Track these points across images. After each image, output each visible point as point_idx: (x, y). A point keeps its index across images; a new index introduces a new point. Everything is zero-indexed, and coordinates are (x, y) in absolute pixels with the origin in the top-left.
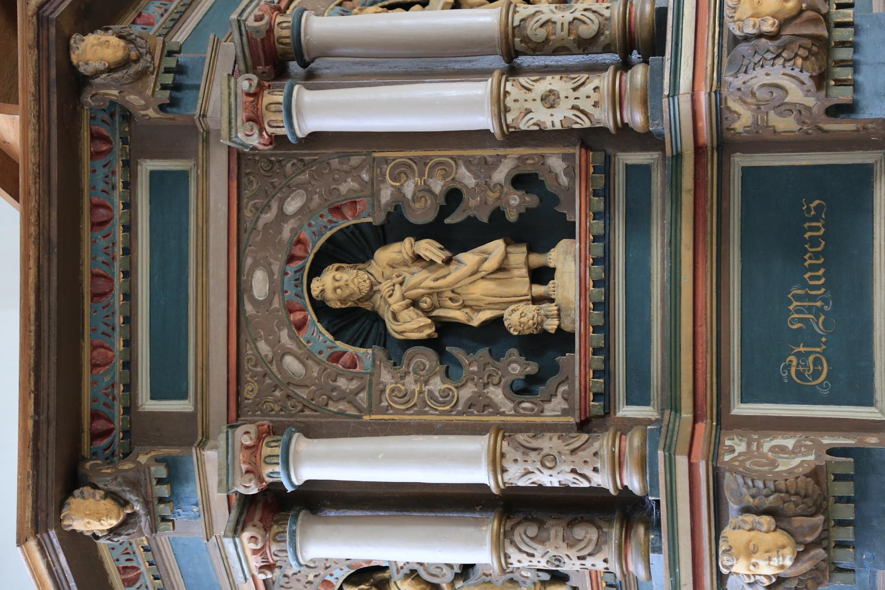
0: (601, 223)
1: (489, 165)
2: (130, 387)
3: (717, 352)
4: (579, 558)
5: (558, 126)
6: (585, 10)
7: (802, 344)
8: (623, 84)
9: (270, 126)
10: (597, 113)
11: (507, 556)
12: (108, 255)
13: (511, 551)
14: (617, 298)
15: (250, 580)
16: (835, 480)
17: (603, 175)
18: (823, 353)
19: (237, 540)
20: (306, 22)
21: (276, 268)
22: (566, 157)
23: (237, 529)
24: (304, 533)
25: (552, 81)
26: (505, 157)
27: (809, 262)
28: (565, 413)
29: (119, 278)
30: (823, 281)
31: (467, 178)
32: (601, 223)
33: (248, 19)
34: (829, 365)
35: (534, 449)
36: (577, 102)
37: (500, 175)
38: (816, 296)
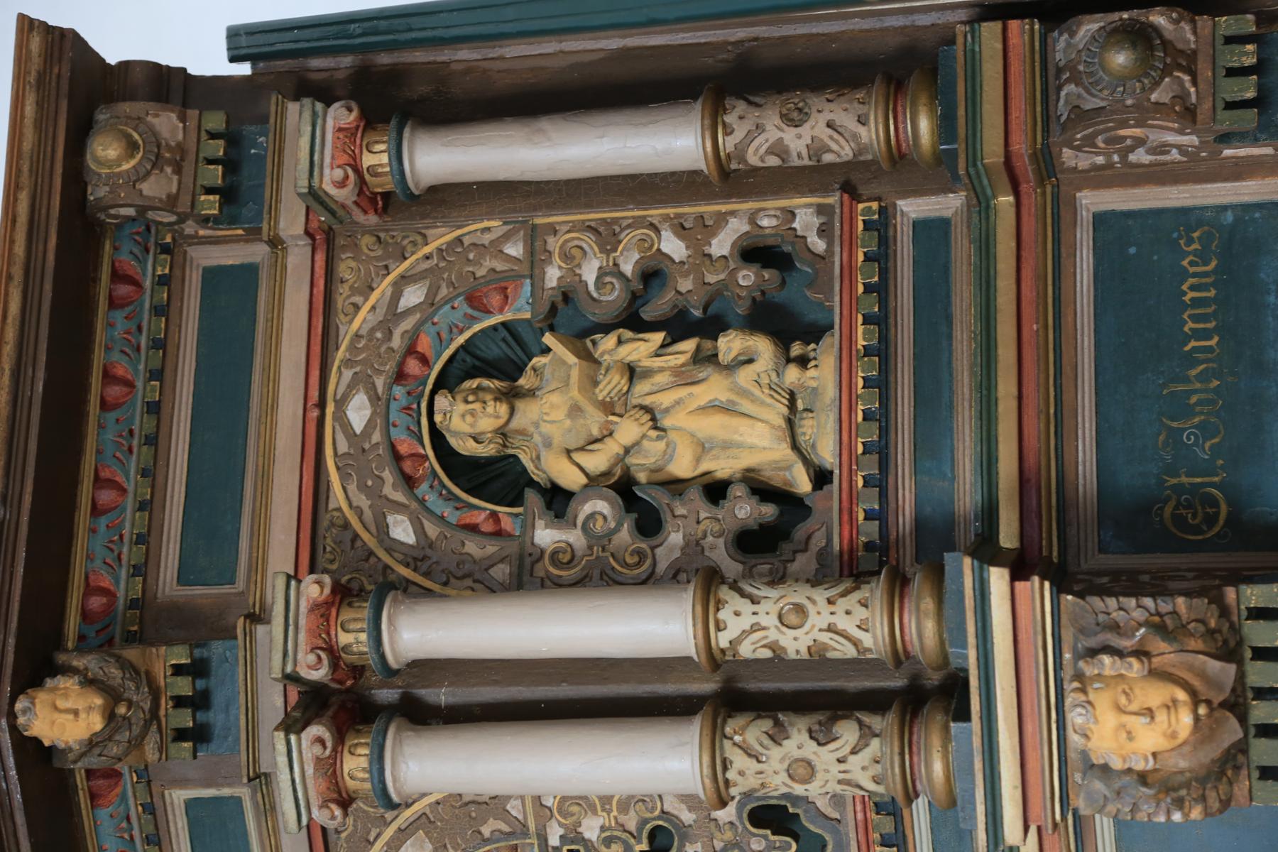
0: (875, 426)
1: (708, 228)
5: (805, 656)
8: (907, 638)
10: (867, 640)
12: (112, 550)
14: (899, 416)
15: (304, 831)
17: (876, 359)
19: (293, 738)
20: (395, 781)
21: (380, 383)
22: (821, 210)
23: (292, 725)
24: (398, 742)
26: (733, 213)
27: (1191, 295)
29: (131, 480)
30: (1212, 293)
31: (673, 246)
33: (313, 816)
35: (778, 600)
36: (832, 619)
37: (721, 245)
38: (1206, 284)
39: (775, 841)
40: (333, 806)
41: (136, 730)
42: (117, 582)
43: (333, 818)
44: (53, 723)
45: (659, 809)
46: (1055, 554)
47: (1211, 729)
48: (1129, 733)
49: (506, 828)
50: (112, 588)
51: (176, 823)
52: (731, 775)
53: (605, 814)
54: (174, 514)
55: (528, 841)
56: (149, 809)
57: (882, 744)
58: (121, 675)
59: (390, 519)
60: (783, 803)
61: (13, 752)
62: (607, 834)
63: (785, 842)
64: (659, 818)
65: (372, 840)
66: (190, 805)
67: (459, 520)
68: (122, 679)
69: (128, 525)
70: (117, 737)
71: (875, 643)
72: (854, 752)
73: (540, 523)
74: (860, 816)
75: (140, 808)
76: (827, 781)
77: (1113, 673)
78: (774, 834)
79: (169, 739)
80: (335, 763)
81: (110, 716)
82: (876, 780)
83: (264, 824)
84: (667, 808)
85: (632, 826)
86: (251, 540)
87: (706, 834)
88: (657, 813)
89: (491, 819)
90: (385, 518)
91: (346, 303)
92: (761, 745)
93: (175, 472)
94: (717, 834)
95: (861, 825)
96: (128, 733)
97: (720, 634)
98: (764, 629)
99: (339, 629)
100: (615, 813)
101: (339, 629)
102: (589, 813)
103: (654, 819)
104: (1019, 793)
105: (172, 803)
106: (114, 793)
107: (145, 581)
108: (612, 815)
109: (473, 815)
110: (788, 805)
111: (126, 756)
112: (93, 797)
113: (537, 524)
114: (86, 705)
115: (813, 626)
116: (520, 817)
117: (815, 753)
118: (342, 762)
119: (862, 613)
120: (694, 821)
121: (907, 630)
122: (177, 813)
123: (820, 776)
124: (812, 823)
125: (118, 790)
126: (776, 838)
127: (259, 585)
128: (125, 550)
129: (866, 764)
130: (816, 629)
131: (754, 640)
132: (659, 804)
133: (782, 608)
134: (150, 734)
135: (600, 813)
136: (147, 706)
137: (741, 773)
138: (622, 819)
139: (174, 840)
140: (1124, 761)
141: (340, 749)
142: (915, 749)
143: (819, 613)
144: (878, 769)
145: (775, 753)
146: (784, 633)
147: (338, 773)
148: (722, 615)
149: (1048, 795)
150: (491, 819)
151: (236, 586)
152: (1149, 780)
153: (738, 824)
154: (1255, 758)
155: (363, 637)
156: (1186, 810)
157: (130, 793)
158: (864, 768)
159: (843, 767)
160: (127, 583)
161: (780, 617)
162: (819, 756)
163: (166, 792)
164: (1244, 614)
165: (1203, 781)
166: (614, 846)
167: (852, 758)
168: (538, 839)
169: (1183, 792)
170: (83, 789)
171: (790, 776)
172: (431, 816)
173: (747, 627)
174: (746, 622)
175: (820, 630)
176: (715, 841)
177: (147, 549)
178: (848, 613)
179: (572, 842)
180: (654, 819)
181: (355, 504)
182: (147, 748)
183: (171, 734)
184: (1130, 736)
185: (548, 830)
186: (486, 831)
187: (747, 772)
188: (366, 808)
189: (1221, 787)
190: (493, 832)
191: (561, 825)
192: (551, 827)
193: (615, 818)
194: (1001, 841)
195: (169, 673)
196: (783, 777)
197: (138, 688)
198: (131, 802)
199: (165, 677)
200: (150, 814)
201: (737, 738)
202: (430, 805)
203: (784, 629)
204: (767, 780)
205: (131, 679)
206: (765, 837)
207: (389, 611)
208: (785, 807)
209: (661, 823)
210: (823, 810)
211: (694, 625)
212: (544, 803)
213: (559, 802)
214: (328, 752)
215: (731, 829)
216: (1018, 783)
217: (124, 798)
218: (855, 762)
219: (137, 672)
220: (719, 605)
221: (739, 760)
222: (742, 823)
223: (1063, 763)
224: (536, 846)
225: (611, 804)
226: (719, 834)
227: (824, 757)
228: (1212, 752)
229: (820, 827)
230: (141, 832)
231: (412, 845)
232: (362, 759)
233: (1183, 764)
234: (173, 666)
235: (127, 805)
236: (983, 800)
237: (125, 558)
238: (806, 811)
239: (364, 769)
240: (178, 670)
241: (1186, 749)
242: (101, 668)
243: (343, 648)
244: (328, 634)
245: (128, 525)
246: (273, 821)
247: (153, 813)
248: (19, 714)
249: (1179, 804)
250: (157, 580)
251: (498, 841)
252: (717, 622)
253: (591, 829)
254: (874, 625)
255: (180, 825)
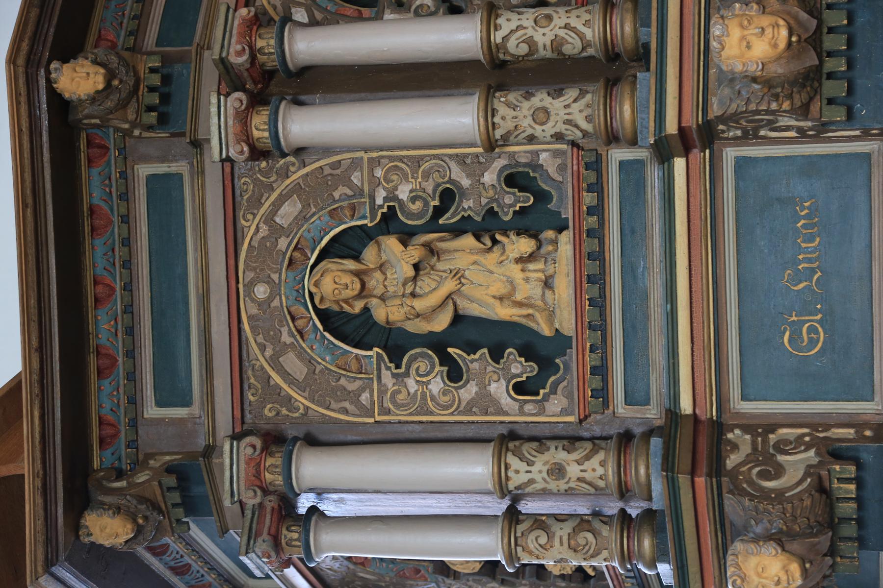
2: (134, 401)
3: (720, 512)
4: (566, 107)
6: (579, 479)
7: (794, 313)
8: (614, 32)
9: (257, 129)
10: (588, 33)
11: (494, 112)
13: (513, 461)
16: (828, 33)
18: (820, 322)
20: (290, 49)
25: (544, 134)
28: (564, 412)
32: (598, 378)
34: (825, 333)
36: (568, 21)
39: (520, 196)
40: (243, 144)
41: (124, 95)
42: (119, 36)
43: (242, 152)
44: (73, 80)
45: (448, 176)
46: (714, 413)
47: (799, 50)
48: (748, 43)
49: (350, 193)
50: (115, 40)
51: (139, 190)
52: (497, 120)
53: (413, 180)
54: (158, 9)
55: (363, 200)
56: (123, 175)
57: (593, 97)
58: (117, 61)
59: (293, 10)
60: (527, 170)
61: (46, 92)
62: (414, 194)
63: (527, 197)
64: (447, 182)
65: (263, 202)
66: (152, 179)
67: (337, 10)
68: (119, 64)
69: (128, 9)
70: (111, 97)
71: (594, 36)
72: (575, 101)
73: (387, 11)
74: (575, 168)
75: (118, 174)
76: (557, 122)
77: (741, 13)
78: (519, 191)
79: (143, 110)
80: (247, 116)
81: (108, 85)
82: (588, 119)
83: (196, 180)
84: (453, 177)
85: (430, 190)
86: (207, 10)
87: (476, 193)
88: (446, 179)
89: (341, 187)
90: (290, 9)
91: (250, 222)
92: (517, 100)
93: (155, 10)
94: (484, 193)
95: (575, 174)
96: (118, 95)
97: (496, 33)
98: (525, 28)
99: (257, 37)
100: (420, 180)
101: (257, 37)
102: (404, 181)
103: (444, 183)
104: (676, 102)
105: (138, 176)
106: (102, 160)
107: (135, 40)
108: (418, 181)
109: (330, 183)
110: (530, 171)
111: (116, 111)
112: (90, 161)
113: (385, 12)
114: (95, 71)
115: (556, 25)
116: (359, 184)
117: (551, 103)
118: (251, 120)
119: (587, 17)
120: (470, 185)
121: (614, 27)
122: (141, 183)
123: (553, 118)
124: (545, 183)
125: (106, 159)
126: (521, 194)
127: (208, 36)
128: (125, 21)
129: (582, 108)
130: (558, 27)
131: (518, 37)
132: (448, 173)
133: (537, 17)
134: (132, 103)
135: (410, 180)
136: (132, 83)
137: (503, 118)
138: (424, 184)
139: (137, 201)
140: (744, 65)
141: (251, 110)
142: (613, 98)
143: (560, 18)
144: (589, 111)
145: (526, 105)
146: (536, 31)
147: (248, 124)
148: (499, 21)
149: (695, 104)
150: (341, 187)
151: (183, 172)
152: (759, 80)
153: (497, 186)
154: (825, 92)
155: (272, 42)
156: (780, 102)
157: (113, 162)
158: (580, 111)
159: (567, 111)
160: (125, 39)
161: (535, 22)
162: (553, 105)
163: (136, 167)
164: (824, 6)
165: (793, 83)
166: (417, 203)
167: (574, 105)
168: (370, 198)
169: (779, 90)
170: (84, 152)
171: (534, 120)
172: (302, 185)
173: (514, 28)
174: (513, 25)
175: (560, 28)
176: (482, 199)
177: (139, 25)
178: (578, 17)
179: (391, 201)
180: (444, 183)
181: (272, 3)
182: (129, 111)
183: (144, 108)
184: (749, 47)
185: (376, 194)
186: (336, 194)
187: (507, 117)
188: (262, 178)
189: (802, 94)
190: (341, 195)
191: (384, 188)
192: (379, 191)
193: (420, 183)
194: (663, 130)
195: (147, 71)
196: (529, 120)
197: (127, 72)
198: (113, 168)
199: (144, 73)
200: (124, 179)
201: (502, 99)
202: (302, 176)
203: (537, 28)
204: (520, 123)
205: (123, 66)
206: (514, 194)
207: (290, 27)
208: (528, 173)
209: (448, 186)
210: (552, 175)
211: (481, 24)
212: (375, 175)
213: (385, 172)
214: (243, 107)
215: (492, 189)
216: (677, 95)
217: (108, 163)
218: (576, 107)
219: (128, 65)
220: (497, 16)
221: (502, 110)
222: (500, 184)
223: (706, 90)
224: (368, 204)
225: (417, 173)
226: (485, 192)
227: (556, 105)
228: (797, 67)
229: (549, 186)
230: (117, 191)
231: (288, 205)
232: (264, 117)
233: (780, 71)
234: (149, 68)
235: (110, 169)
236: (654, 102)
237: (124, 25)
238: (541, 175)
239: (265, 123)
240: (153, 70)
241: (783, 61)
242: (106, 55)
243: (259, 50)
244: (250, 38)
245: (128, 9)
246: (202, 181)
247: (126, 179)
248: (52, 71)
249: (776, 97)
250: (144, 41)
251: (344, 200)
252: (493, 124)
253: (404, 192)
254: (594, 23)
255: (142, 192)
